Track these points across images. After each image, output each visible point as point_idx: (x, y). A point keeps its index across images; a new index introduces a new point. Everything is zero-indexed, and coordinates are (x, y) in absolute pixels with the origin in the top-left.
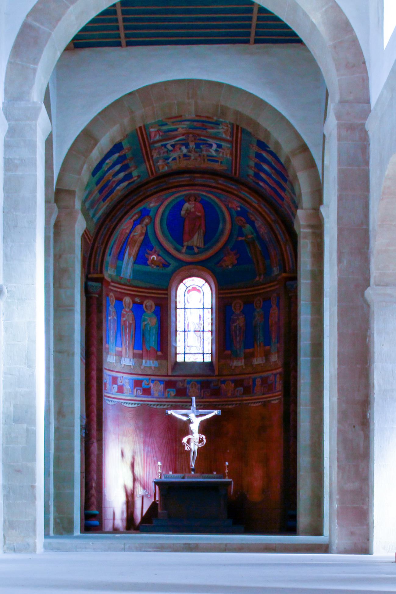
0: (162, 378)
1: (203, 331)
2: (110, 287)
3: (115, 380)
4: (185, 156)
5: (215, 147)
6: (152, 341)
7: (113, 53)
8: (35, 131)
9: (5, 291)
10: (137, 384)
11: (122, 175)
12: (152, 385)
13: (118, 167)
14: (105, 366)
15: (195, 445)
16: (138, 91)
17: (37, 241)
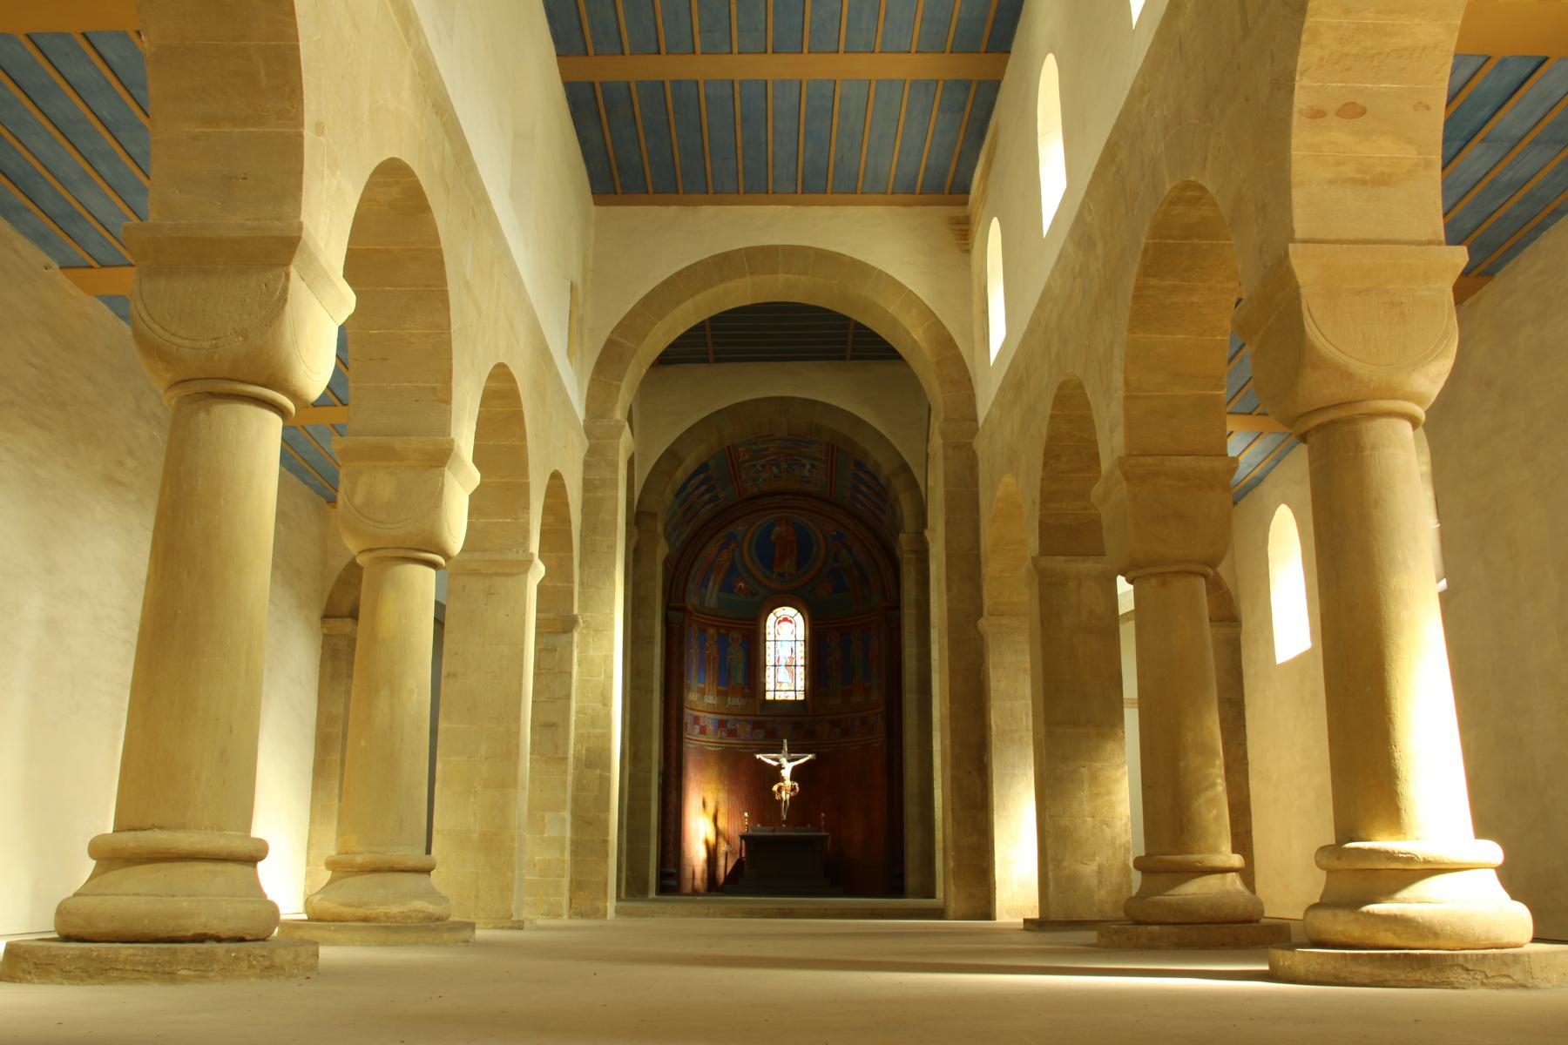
0: (750, 718)
1: (795, 666)
2: (694, 618)
3: (696, 720)
4: (775, 476)
5: (808, 467)
6: (739, 677)
7: (701, 370)
8: (618, 451)
9: (581, 621)
10: (721, 724)
11: (707, 497)
12: (738, 725)
13: (703, 488)
14: (686, 704)
15: (786, 793)
16: (726, 408)
17: (617, 567)
